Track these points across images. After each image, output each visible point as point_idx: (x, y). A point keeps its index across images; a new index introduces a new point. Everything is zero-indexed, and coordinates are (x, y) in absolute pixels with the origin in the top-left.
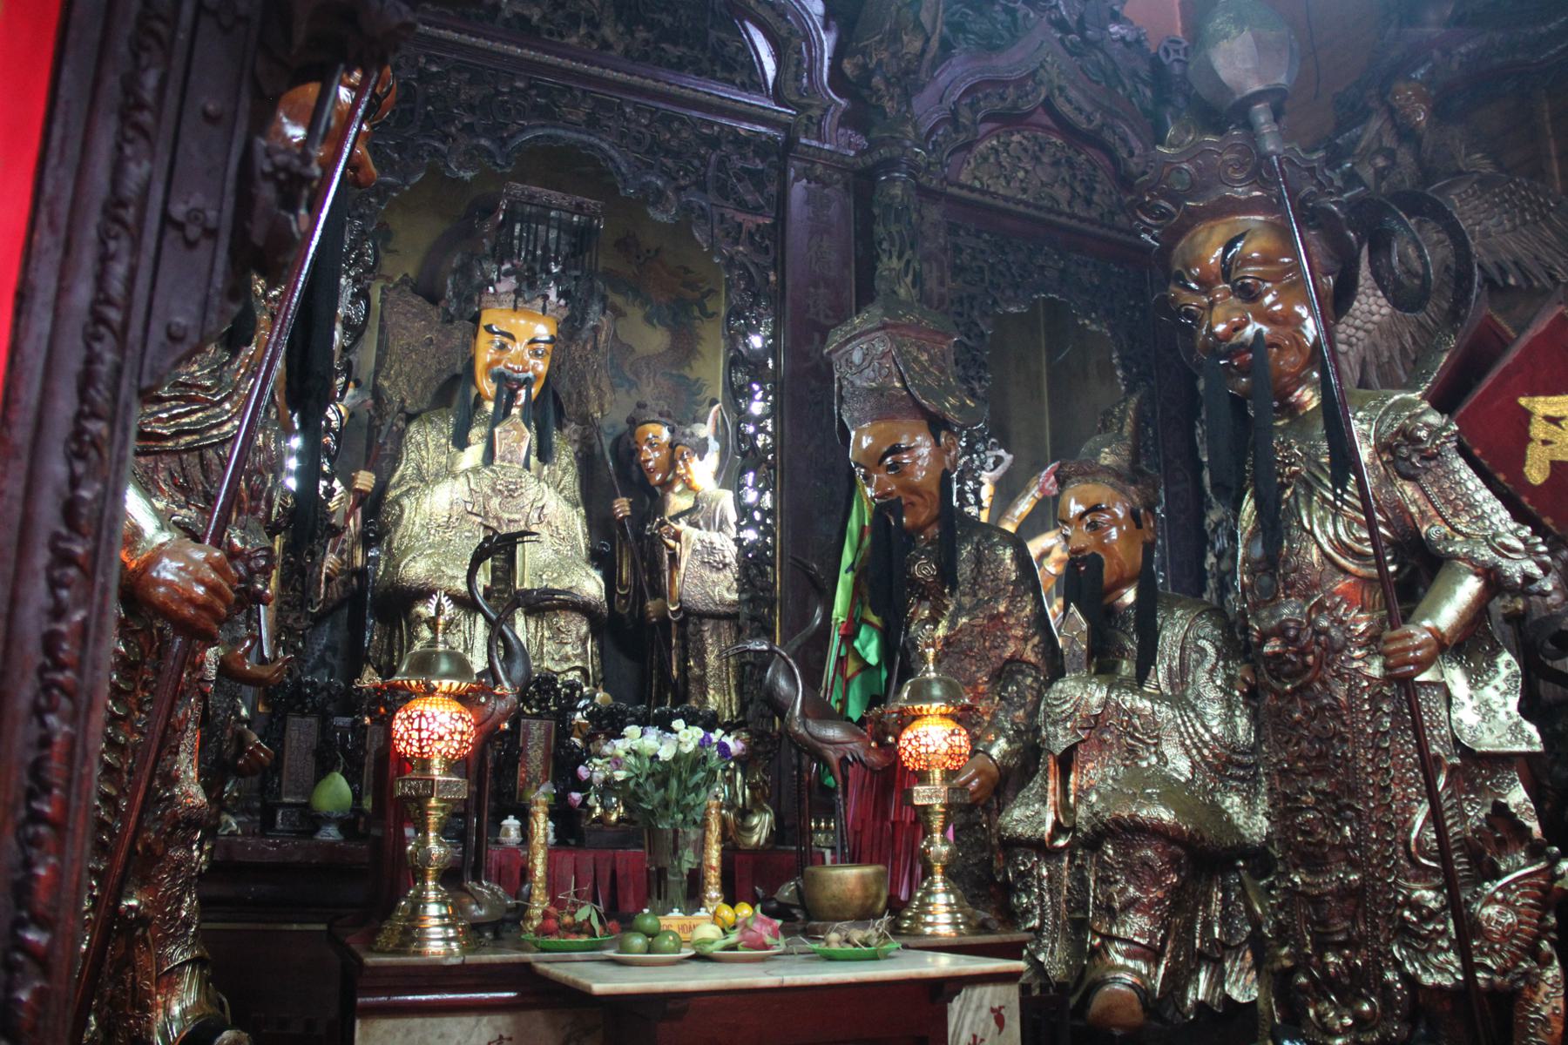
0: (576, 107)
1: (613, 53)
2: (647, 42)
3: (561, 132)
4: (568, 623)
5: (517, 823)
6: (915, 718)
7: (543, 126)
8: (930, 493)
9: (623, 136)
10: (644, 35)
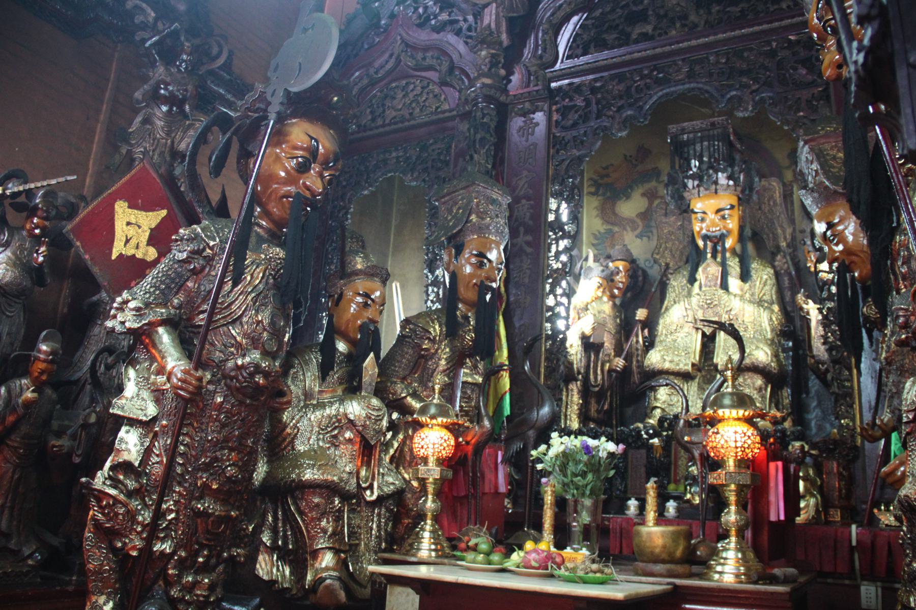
0: (679, 70)
1: (699, 29)
2: (719, 11)
3: (672, 89)
4: (745, 380)
5: (636, 503)
6: (720, 421)
7: (661, 90)
8: (862, 251)
9: (711, 75)
10: (717, 8)
